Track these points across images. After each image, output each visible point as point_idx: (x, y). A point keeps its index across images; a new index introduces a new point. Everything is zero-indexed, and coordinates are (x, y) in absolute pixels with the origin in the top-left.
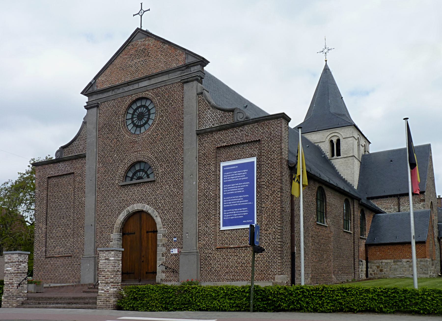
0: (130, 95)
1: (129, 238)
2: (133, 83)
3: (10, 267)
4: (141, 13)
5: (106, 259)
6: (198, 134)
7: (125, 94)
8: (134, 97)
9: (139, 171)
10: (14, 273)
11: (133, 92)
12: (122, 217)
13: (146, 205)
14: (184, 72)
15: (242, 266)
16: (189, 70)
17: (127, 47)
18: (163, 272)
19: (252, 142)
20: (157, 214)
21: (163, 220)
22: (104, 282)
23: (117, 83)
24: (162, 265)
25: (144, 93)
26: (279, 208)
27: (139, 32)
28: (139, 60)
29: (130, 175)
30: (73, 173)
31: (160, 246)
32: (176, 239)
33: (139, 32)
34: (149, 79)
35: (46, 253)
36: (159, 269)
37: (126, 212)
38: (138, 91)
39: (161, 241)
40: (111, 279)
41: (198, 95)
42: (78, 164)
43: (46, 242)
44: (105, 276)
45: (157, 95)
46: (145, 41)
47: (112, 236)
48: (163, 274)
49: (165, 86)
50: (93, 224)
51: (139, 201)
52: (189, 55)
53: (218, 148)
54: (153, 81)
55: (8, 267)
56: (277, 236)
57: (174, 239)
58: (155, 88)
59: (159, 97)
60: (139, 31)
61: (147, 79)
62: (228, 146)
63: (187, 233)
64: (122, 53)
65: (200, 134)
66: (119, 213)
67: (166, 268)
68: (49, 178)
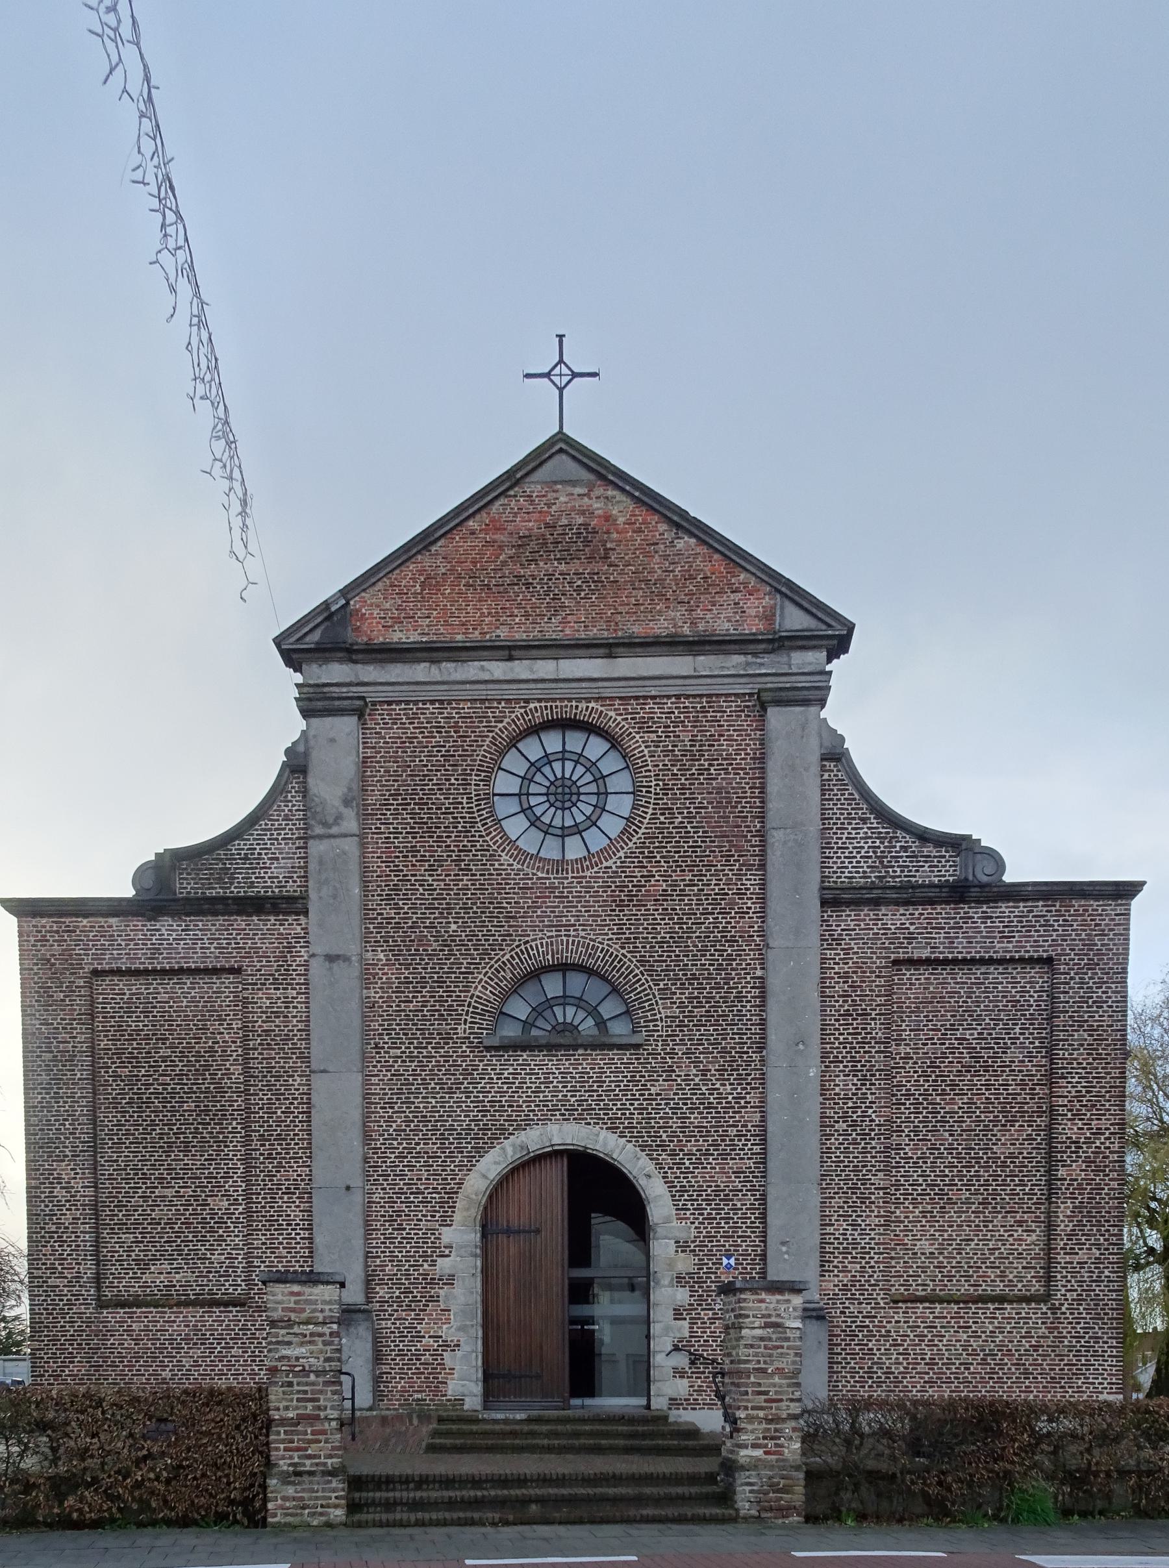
0: (517, 701)
1: (511, 1248)
2: (534, 652)
3: (302, 1344)
4: (561, 375)
5: (767, 1325)
6: (824, 903)
7: (493, 692)
8: (539, 712)
9: (564, 1000)
10: (318, 1373)
11: (535, 691)
12: (492, 1164)
13: (604, 1133)
14: (762, 664)
15: (984, 1362)
16: (785, 659)
17: (502, 501)
18: (679, 1373)
19: (1022, 960)
20: (650, 1167)
21: (677, 1192)
22: (761, 1414)
23: (459, 637)
24: (676, 1348)
25: (583, 705)
26: (1114, 1184)
27: (561, 450)
28: (563, 567)
29: (519, 1009)
30: (236, 971)
31: (666, 1282)
32: (732, 1261)
33: (561, 450)
34: (610, 656)
35: (98, 1289)
36: (663, 1361)
37: (510, 1151)
38: (562, 690)
39: (671, 1264)
40: (792, 1405)
41: (822, 760)
42: (263, 932)
43: (97, 1243)
44: (766, 1393)
45: (643, 726)
46: (588, 495)
47: (448, 1235)
48: (678, 1381)
49: (678, 697)
50: (356, 1182)
51: (572, 1114)
52: (787, 603)
53: (896, 962)
54: (625, 666)
55: (289, 1343)
56: (1107, 1273)
57: (725, 1261)
58: (637, 698)
59: (653, 736)
60: (560, 445)
61: (602, 651)
62: (937, 962)
63: (783, 1243)
64: (478, 517)
65: (833, 900)
66: (480, 1151)
67: (692, 1363)
68: (96, 973)
